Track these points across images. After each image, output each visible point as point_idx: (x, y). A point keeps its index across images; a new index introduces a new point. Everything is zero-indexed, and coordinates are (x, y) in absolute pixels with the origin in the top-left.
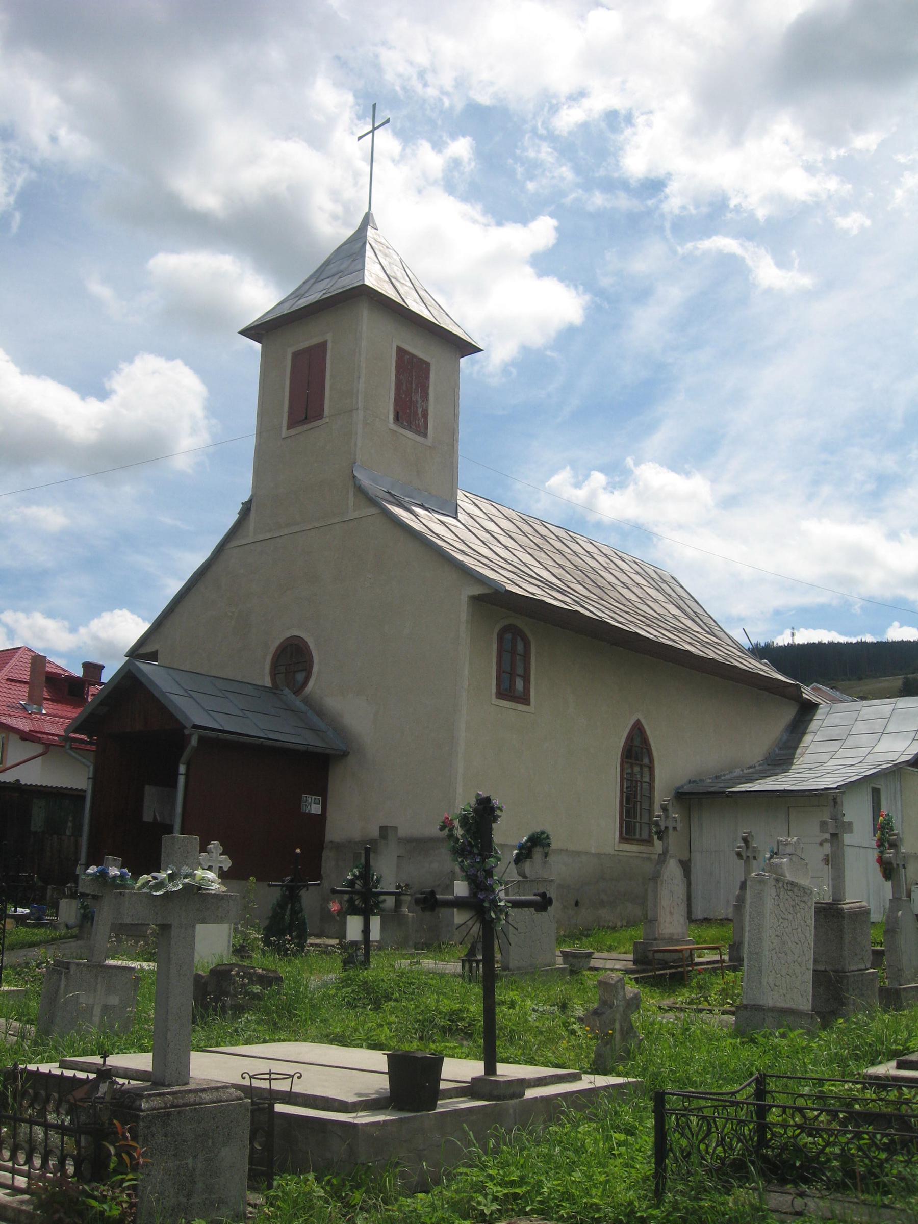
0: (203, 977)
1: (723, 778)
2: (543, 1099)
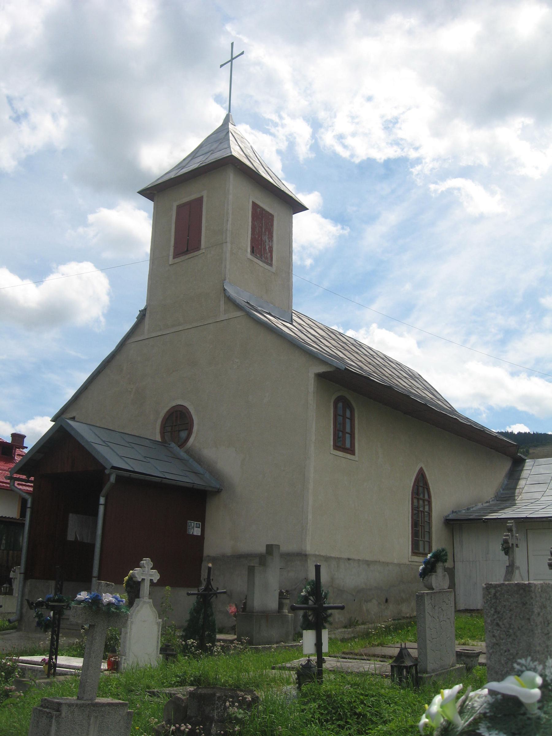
0: (183, 700)
1: (471, 509)
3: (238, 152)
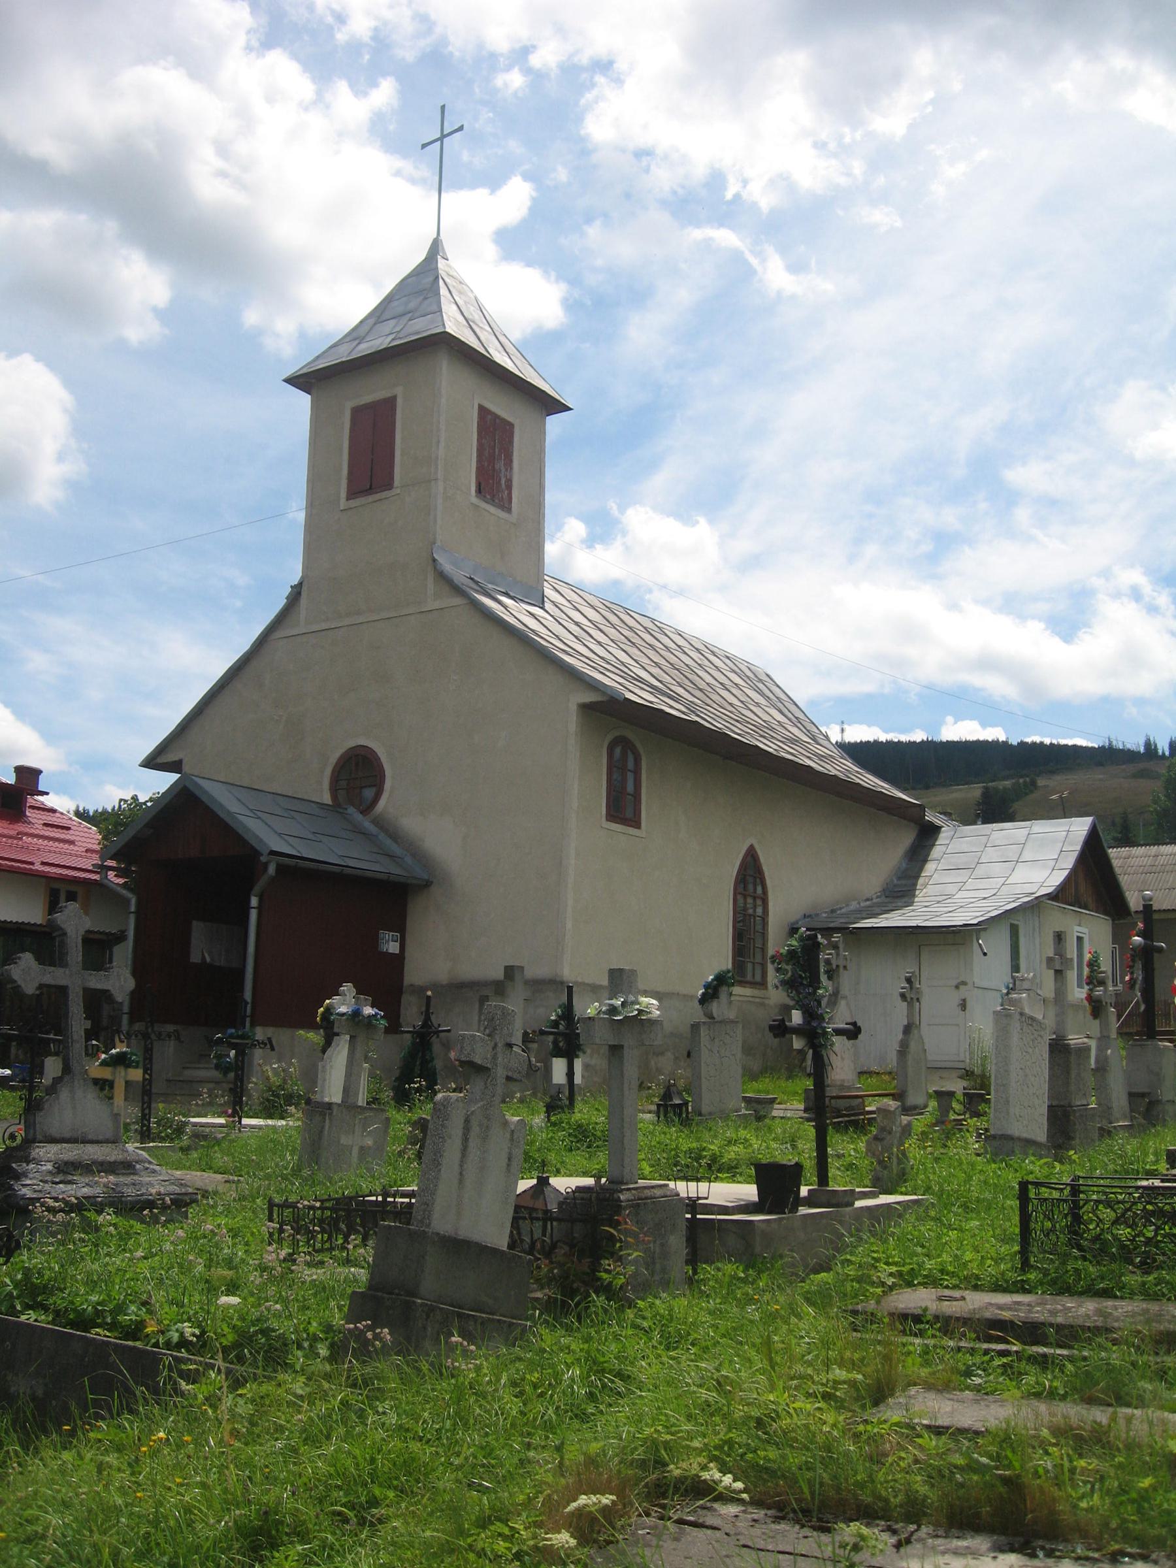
2: (868, 1208)
3: (455, 319)
